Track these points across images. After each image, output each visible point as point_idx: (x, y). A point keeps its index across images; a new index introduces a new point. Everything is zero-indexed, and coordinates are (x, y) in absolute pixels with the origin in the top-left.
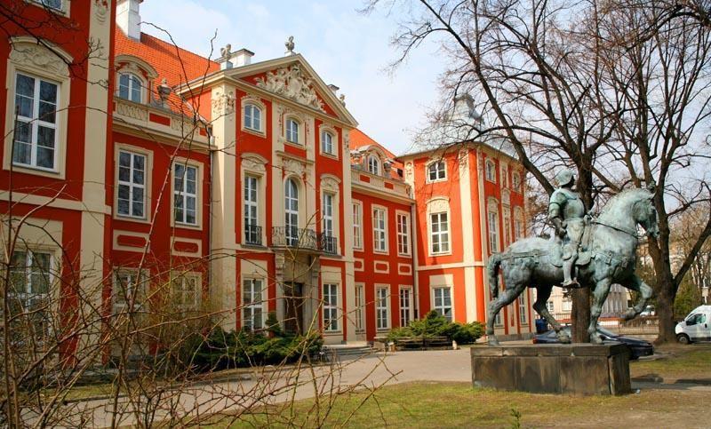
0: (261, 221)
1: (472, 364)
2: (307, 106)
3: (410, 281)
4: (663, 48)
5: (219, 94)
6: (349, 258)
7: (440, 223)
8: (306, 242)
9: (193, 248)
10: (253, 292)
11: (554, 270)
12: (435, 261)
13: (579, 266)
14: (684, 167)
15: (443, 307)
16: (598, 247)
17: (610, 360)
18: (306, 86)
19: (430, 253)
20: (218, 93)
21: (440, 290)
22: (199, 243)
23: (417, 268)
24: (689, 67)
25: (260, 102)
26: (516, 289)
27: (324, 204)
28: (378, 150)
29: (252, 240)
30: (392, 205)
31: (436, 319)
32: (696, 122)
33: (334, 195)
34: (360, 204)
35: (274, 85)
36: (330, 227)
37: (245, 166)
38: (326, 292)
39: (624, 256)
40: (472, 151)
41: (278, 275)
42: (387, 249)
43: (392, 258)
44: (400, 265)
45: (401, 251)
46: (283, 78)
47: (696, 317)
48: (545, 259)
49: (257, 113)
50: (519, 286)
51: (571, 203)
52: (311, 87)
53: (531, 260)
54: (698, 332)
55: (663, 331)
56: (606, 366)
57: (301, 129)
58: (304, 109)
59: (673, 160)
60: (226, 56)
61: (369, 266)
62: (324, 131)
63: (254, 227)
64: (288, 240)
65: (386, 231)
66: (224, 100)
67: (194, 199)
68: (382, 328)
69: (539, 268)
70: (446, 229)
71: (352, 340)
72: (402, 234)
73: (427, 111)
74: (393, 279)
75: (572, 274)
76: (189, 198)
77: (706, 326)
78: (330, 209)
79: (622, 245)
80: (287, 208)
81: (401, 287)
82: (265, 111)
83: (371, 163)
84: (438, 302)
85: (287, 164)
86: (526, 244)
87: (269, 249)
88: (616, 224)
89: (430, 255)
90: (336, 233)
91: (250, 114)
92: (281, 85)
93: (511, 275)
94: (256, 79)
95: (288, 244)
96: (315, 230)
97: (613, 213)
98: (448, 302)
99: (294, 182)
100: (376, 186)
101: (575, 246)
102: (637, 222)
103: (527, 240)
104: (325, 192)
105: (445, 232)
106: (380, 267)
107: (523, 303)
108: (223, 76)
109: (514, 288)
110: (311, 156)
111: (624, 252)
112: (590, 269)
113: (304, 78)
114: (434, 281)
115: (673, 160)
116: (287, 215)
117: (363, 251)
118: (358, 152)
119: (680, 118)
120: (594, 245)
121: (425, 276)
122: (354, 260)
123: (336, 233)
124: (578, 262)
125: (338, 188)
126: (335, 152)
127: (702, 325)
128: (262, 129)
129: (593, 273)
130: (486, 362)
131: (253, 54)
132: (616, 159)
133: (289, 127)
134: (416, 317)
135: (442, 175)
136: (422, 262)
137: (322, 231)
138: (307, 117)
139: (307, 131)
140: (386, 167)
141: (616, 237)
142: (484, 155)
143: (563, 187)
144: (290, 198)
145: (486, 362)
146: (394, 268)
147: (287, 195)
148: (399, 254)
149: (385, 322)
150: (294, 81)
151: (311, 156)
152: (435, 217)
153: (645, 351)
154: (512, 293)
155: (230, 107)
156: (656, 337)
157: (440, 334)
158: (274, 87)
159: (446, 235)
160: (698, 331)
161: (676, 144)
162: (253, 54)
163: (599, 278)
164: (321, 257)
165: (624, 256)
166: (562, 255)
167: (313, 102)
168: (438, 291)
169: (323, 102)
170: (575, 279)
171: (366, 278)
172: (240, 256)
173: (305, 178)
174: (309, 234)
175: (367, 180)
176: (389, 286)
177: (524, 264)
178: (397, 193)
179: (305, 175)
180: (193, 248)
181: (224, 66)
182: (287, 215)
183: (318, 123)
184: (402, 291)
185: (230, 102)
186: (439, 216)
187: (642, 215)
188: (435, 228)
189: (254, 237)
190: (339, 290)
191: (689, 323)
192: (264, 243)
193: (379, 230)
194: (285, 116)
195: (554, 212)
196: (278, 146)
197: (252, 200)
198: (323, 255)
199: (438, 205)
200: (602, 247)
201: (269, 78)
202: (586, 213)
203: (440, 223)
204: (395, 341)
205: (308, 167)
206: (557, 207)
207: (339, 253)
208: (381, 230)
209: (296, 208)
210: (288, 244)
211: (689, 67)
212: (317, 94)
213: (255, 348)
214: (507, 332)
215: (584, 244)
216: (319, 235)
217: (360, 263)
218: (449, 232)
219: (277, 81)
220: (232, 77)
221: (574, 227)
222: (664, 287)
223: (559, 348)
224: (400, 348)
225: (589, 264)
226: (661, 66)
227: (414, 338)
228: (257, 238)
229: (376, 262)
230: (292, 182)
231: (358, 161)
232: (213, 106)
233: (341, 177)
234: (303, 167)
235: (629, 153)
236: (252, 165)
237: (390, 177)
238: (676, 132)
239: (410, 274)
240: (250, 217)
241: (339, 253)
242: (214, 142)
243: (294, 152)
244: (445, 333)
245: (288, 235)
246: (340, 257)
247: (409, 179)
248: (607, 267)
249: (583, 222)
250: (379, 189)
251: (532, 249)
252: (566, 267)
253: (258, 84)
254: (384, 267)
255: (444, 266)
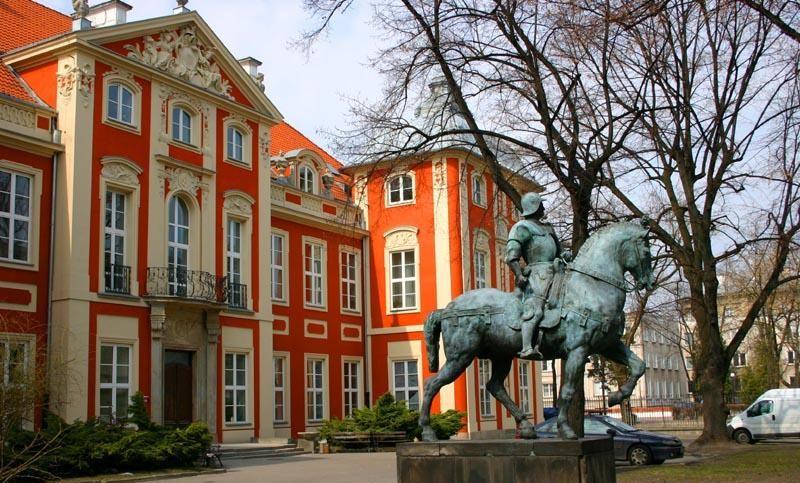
0: (130, 258)
1: (398, 474)
2: (205, 90)
3: (359, 349)
4: (712, 26)
5: (68, 66)
6: (265, 314)
7: (403, 265)
8: (195, 289)
9: (24, 298)
10: (115, 364)
11: (511, 334)
12: (396, 320)
13: (545, 330)
14: (737, 191)
15: (407, 389)
16: (571, 303)
17: (583, 461)
18: (204, 60)
19: (389, 308)
20: (66, 66)
21: (232, 355)
22: (33, 290)
23: (371, 331)
24: (744, 56)
25: (132, 82)
26: (460, 361)
27: (229, 235)
28: (315, 155)
29: (114, 288)
30: (334, 238)
31: (391, 406)
32: (756, 128)
33: (244, 222)
34: (286, 236)
35: (155, 57)
36: (237, 269)
37: (108, 176)
38: (229, 364)
39: (605, 315)
40: (453, 162)
41: (155, 339)
42: (324, 303)
43: (333, 316)
44: (343, 326)
45: (345, 305)
46: (169, 46)
47: (760, 405)
48: (499, 319)
49: (127, 98)
50: (465, 356)
51: (537, 241)
52: (212, 61)
53: (481, 320)
54: (762, 425)
55: (709, 426)
56: (576, 468)
57: (195, 122)
58: (202, 94)
59: (724, 182)
60: (80, 10)
61: (297, 327)
62: (232, 127)
63: (119, 267)
64: (172, 286)
65: (323, 275)
66: (76, 76)
67: (27, 223)
68: (315, 419)
69: (491, 331)
70: (413, 275)
71: (267, 438)
72: (348, 280)
73: (353, 104)
74: (333, 347)
75: (534, 341)
76: (173, 222)
77: (774, 417)
78: (237, 242)
79: (603, 301)
80: (172, 239)
81: (344, 359)
82: (139, 95)
83: (302, 175)
84: (400, 382)
85: (172, 174)
86: (475, 298)
87: (142, 300)
88: (595, 270)
89: (388, 313)
90: (245, 278)
91: (116, 100)
92: (165, 56)
93: (452, 341)
94: (127, 46)
95: (172, 293)
96: (213, 272)
97: (592, 256)
98: (414, 381)
99: (183, 200)
100: (310, 210)
101: (540, 301)
102: (625, 269)
103: (476, 292)
104: (230, 218)
105: (411, 279)
106: (313, 329)
107: (525, 384)
108: (75, 41)
109: (457, 360)
110: (209, 163)
111: (606, 310)
112: (560, 333)
113: (202, 48)
114: (395, 350)
115: (724, 182)
116: (171, 250)
117: (288, 305)
118: (283, 159)
119: (733, 122)
120: (566, 300)
121: (381, 343)
122: (272, 318)
123: (245, 278)
124: (543, 324)
125: (250, 211)
126: (247, 158)
127: (769, 416)
128: (136, 121)
129: (564, 339)
130: (416, 464)
131: (130, 8)
132: (651, 178)
133: (176, 119)
134: (367, 403)
135: (408, 195)
136: (377, 323)
137: (225, 274)
138: (205, 105)
139: (204, 126)
140: (325, 181)
141: (594, 289)
142: (470, 168)
143: (527, 217)
144: (176, 225)
145: (416, 464)
146: (334, 331)
147: (172, 220)
148: (306, 305)
149: (319, 409)
150: (187, 51)
151: (209, 163)
152: (396, 257)
153: (669, 451)
154: (453, 366)
155: (86, 88)
156: (699, 433)
157: (395, 428)
158: (154, 60)
159: (413, 283)
160: (764, 425)
161: (729, 160)
162: (130, 8)
163: (571, 348)
164: (222, 314)
165: (605, 315)
166: (522, 314)
167: (214, 84)
168: (399, 365)
169: (230, 83)
170: (537, 347)
171: (291, 344)
172: (96, 309)
173: (199, 198)
174: (203, 279)
175: (296, 200)
176: (327, 357)
177: (471, 325)
178: (341, 220)
179: (199, 192)
180: (24, 298)
181: (76, 26)
182: (171, 250)
183: (221, 114)
184: (346, 365)
185: (86, 80)
186: (403, 254)
187: (631, 259)
188: (397, 273)
189: (119, 282)
190: (249, 362)
191: (751, 414)
192: (135, 291)
193: (313, 274)
194: (171, 103)
195: (513, 253)
196: (158, 147)
197: (117, 227)
198: (224, 310)
199: (401, 239)
200: (577, 303)
201: (148, 45)
202: (558, 255)
203: (403, 265)
204: (329, 438)
205: (204, 179)
206: (517, 245)
207: (250, 307)
208: (317, 275)
209: (188, 242)
210: (172, 293)
211: (744, 56)
212: (221, 72)
213: (105, 447)
214: (500, 426)
215: (552, 299)
216: (220, 280)
217: (283, 322)
218: (416, 279)
219: (159, 50)
220: (88, 42)
221: (539, 275)
222: (711, 361)
223: (514, 445)
224: (336, 448)
225: (558, 326)
226: (709, 49)
227: (359, 434)
228: (125, 284)
229: (307, 322)
230: (181, 202)
231: (283, 172)
232: (59, 84)
233: (255, 196)
234: (197, 179)
235: (669, 170)
236: (120, 173)
237: (332, 197)
238: (728, 143)
239: (359, 339)
240: (113, 253)
241: (250, 307)
242: (59, 138)
243: (184, 157)
244: (404, 426)
245: (171, 280)
246: (252, 314)
247: (361, 201)
248: (582, 332)
249: (553, 268)
250: (314, 213)
251: (482, 304)
252: (527, 329)
253: (130, 55)
254: (319, 329)
255: (409, 329)
